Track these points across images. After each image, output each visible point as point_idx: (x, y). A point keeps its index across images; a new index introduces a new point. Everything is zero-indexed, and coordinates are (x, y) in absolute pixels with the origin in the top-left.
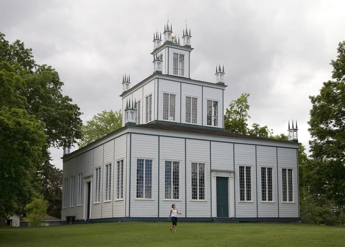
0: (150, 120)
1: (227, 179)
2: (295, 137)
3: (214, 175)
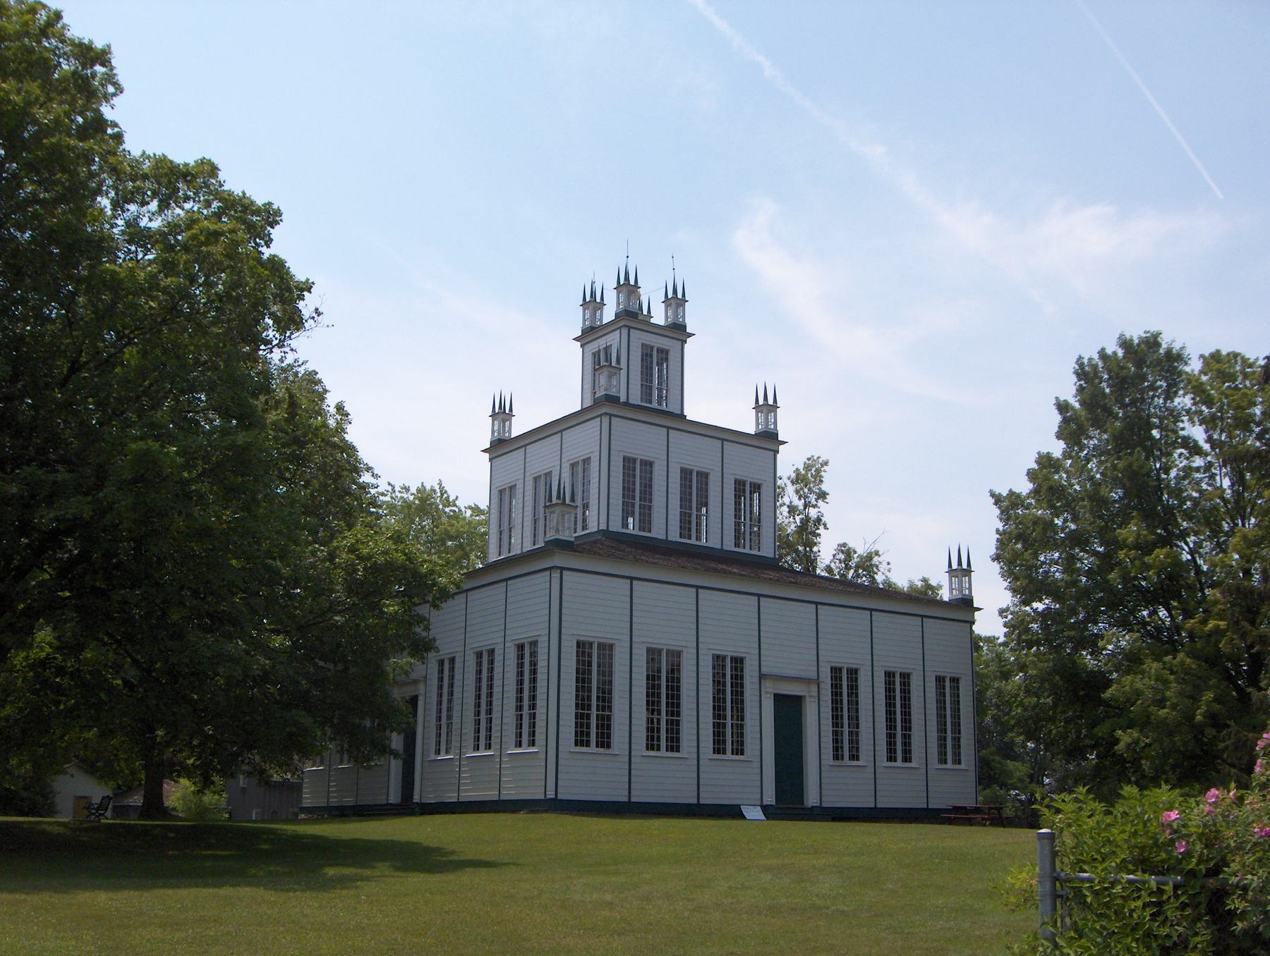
0: (584, 528)
1: (797, 701)
2: (967, 592)
3: (770, 688)
